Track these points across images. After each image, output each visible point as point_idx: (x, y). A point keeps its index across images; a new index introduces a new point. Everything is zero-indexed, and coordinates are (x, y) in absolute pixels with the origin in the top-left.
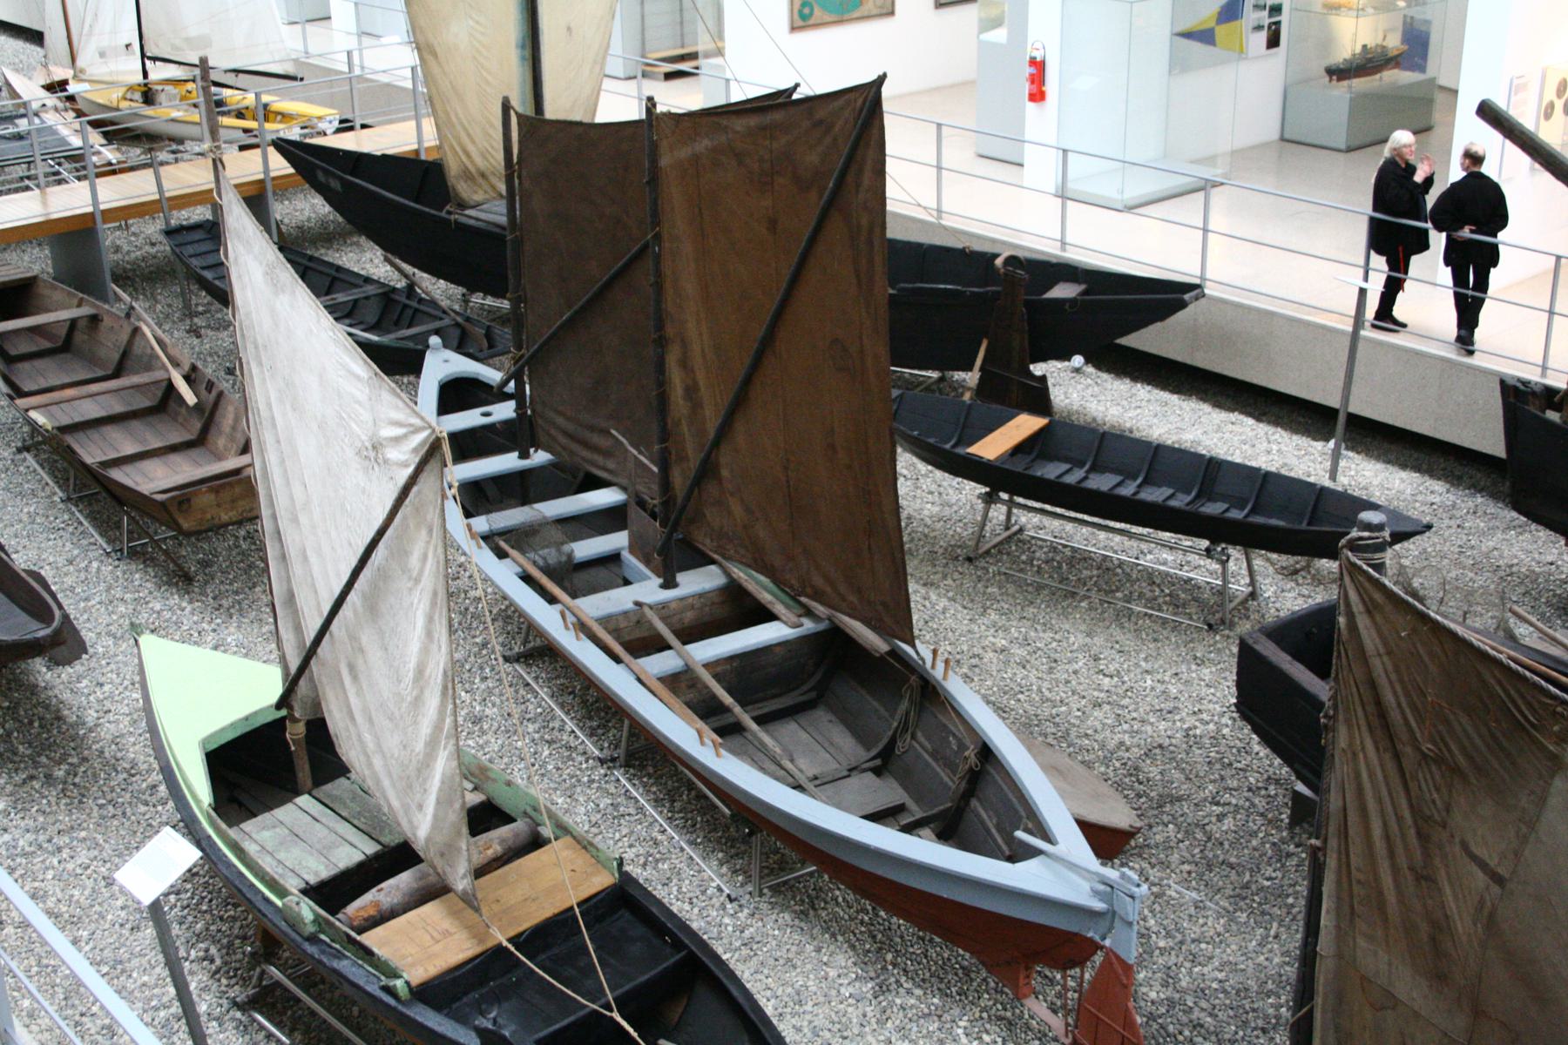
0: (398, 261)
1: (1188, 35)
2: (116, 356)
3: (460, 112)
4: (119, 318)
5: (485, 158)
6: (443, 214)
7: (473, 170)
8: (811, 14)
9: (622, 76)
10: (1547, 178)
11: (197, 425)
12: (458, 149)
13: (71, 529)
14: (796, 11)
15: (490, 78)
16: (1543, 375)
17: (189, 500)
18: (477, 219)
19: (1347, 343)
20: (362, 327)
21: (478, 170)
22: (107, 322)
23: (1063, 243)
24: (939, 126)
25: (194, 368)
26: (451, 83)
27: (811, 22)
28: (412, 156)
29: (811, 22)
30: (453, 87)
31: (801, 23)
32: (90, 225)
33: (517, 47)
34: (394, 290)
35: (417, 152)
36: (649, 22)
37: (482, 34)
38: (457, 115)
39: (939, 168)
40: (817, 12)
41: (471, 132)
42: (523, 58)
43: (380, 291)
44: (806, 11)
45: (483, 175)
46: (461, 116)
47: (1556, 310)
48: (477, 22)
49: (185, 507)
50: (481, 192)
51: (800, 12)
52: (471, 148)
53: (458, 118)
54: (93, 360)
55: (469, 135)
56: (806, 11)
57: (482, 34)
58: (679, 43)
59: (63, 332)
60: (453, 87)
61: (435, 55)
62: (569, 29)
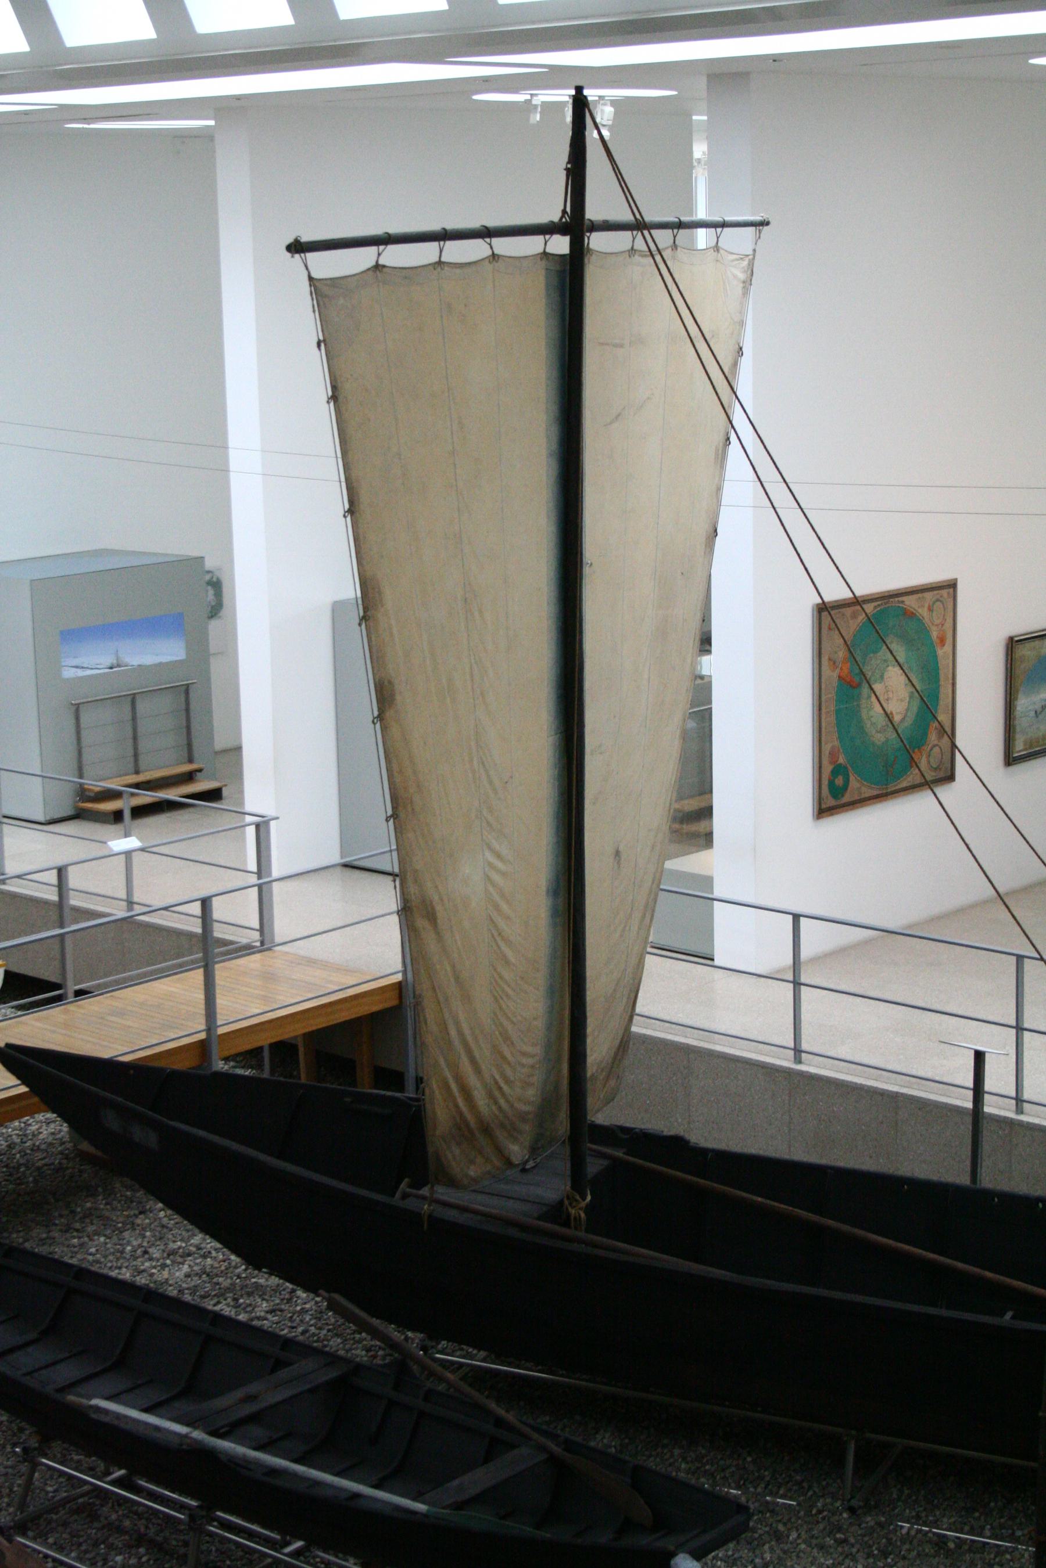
0: (376, 1322)
1: (221, 653)
3: (462, 1017)
5: (491, 1096)
6: (396, 1200)
8: (845, 787)
9: (41, 818)
10: (1042, 864)
12: (454, 1086)
14: (825, 782)
15: (509, 954)
18: (464, 1209)
19: (969, 1120)
20: (257, 1431)
21: (480, 1120)
23: (798, 1052)
24: (796, 917)
26: (453, 967)
27: (846, 799)
28: (182, 1065)
29: (846, 799)
30: (457, 979)
31: (831, 802)
33: (548, 891)
34: (358, 1368)
35: (202, 1048)
36: (87, 737)
37: (504, 874)
38: (457, 1024)
39: (1020, 1028)
40: (854, 783)
41: (476, 1054)
42: (555, 913)
43: (333, 1374)
44: (839, 781)
45: (486, 1130)
46: (467, 1032)
47: (1026, 1025)
48: (499, 856)
50: (480, 1160)
51: (831, 783)
52: (473, 1080)
53: (461, 1033)
55: (473, 1061)
56: (839, 781)
57: (504, 874)
58: (131, 766)
60: (457, 979)
61: (432, 917)
62: (617, 853)
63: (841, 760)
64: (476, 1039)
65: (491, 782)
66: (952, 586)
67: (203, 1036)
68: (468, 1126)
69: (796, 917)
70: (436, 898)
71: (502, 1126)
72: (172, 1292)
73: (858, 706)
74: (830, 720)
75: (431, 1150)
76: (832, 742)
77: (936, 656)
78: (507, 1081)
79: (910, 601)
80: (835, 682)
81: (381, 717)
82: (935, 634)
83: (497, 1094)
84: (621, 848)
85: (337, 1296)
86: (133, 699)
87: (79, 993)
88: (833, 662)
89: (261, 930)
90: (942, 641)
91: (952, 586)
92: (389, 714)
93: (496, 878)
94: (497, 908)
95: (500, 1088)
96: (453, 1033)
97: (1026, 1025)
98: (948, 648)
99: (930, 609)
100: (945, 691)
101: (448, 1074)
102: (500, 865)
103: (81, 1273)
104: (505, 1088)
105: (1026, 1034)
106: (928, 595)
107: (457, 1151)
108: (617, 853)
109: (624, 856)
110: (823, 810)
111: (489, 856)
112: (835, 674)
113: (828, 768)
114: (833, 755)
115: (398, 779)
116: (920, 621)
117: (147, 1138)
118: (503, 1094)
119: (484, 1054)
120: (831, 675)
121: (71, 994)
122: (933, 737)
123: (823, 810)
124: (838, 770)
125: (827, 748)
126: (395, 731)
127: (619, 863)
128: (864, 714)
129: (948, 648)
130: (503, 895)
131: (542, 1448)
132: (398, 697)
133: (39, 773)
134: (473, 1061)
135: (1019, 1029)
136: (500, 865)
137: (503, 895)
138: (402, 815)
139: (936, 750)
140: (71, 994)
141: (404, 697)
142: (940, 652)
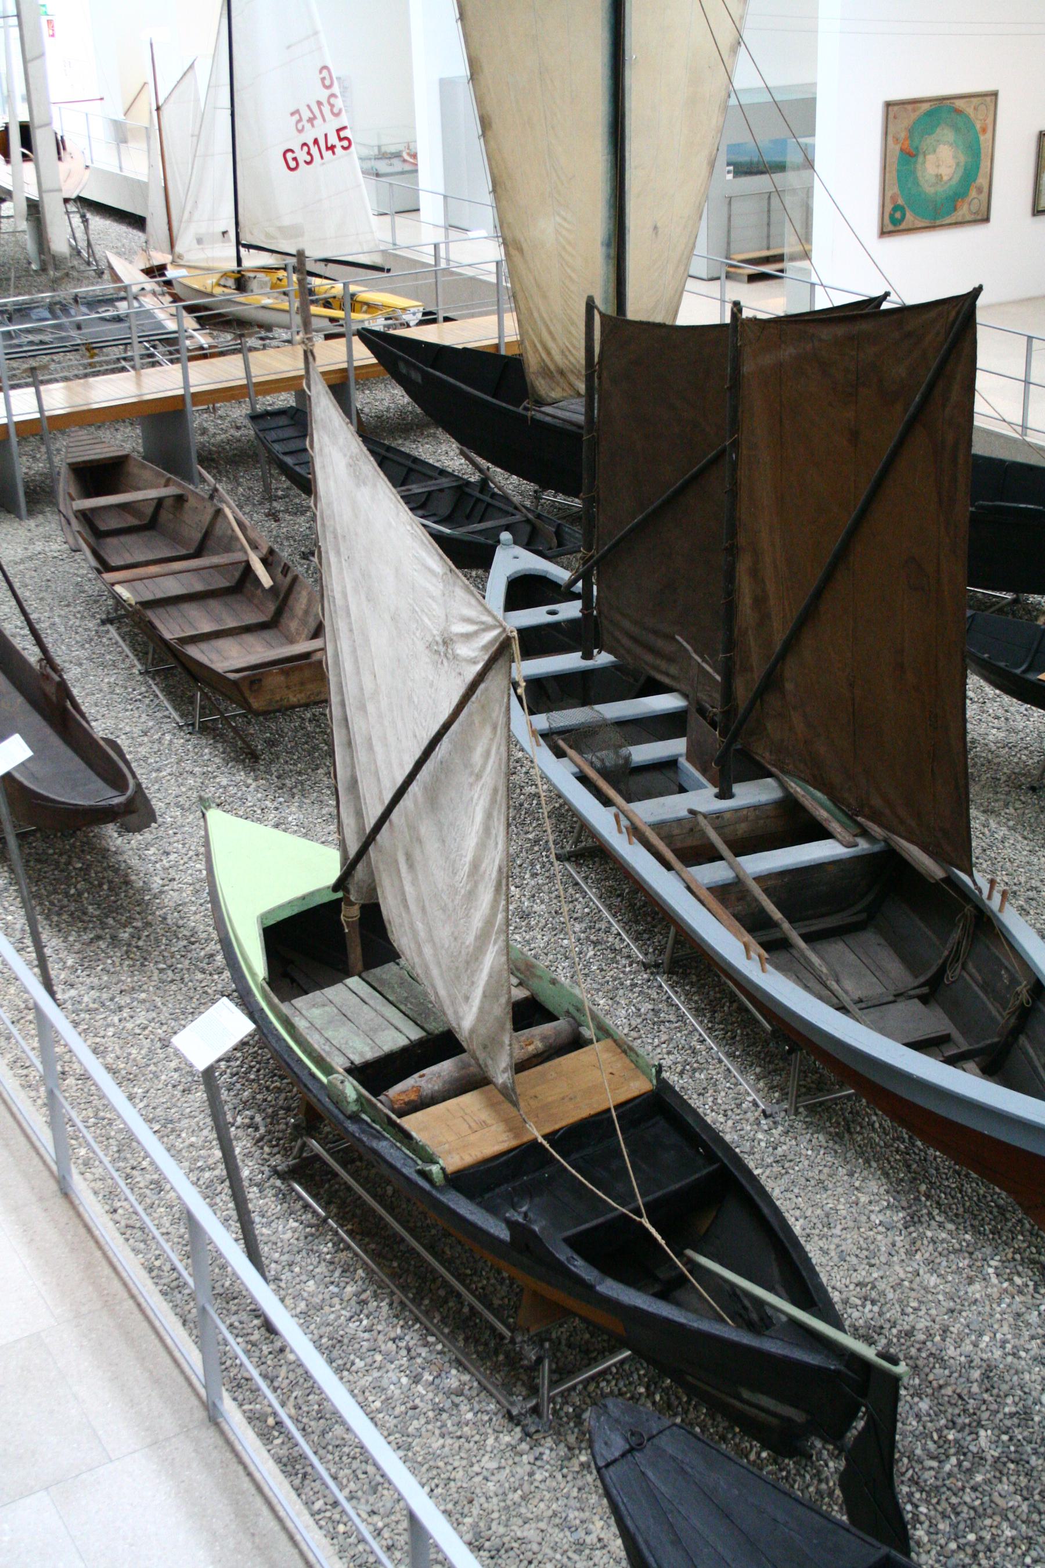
2: (198, 536)
3: (542, 308)
4: (203, 498)
5: (563, 353)
6: (520, 410)
7: (552, 367)
11: (271, 607)
13: (147, 701)
15: (573, 275)
16: (1024, 434)
17: (260, 680)
22: (192, 502)
24: (1030, 338)
25: (271, 551)
29: (903, 226)
31: (891, 228)
32: (180, 408)
34: (468, 483)
35: (497, 346)
38: (539, 310)
40: (909, 216)
41: (552, 328)
42: (608, 256)
45: (562, 373)
46: (545, 316)
48: (565, 220)
49: (256, 687)
50: (559, 389)
51: (891, 216)
52: (551, 344)
54: (175, 538)
55: (550, 333)
56: (898, 215)
59: (149, 510)
61: (521, 250)
62: (655, 228)
63: (900, 202)
64: (551, 320)
65: (559, 178)
66: (995, 94)
67: (496, 341)
68: (549, 369)
69: (1030, 338)
70: (522, 240)
71: (572, 372)
72: (450, 470)
73: (915, 168)
74: (892, 176)
75: (528, 381)
76: (893, 190)
77: (978, 141)
78: (574, 347)
79: (959, 104)
80: (897, 152)
81: (484, 134)
82: (978, 127)
83: (567, 353)
84: (659, 225)
85: (465, 449)
86: (731, 198)
87: (447, 319)
88: (896, 140)
89: (435, 256)
90: (984, 130)
91: (995, 94)
92: (489, 133)
93: (564, 232)
94: (564, 248)
95: (570, 351)
96: (536, 314)
97: (1032, 380)
98: (989, 135)
99: (976, 109)
100: (985, 164)
101: (534, 337)
102: (566, 225)
103: (416, 460)
104: (574, 351)
105: (1031, 386)
106: (975, 100)
107: (543, 382)
108: (655, 228)
109: (660, 231)
110: (883, 233)
111: (558, 219)
112: (898, 147)
113: (889, 207)
114: (893, 198)
115: (496, 171)
116: (967, 117)
117: (417, 377)
118: (572, 354)
119: (557, 329)
120: (895, 149)
121: (441, 319)
122: (973, 193)
123: (883, 233)
124: (896, 208)
125: (889, 194)
126: (492, 143)
127: (656, 234)
128: (919, 174)
129: (989, 135)
130: (569, 243)
131: (526, 516)
132: (494, 126)
133: (705, 254)
134: (550, 333)
135: (1027, 382)
136: (566, 225)
137: (569, 243)
138: (499, 190)
139: (976, 201)
140: (441, 319)
141: (497, 124)
142: (982, 138)
